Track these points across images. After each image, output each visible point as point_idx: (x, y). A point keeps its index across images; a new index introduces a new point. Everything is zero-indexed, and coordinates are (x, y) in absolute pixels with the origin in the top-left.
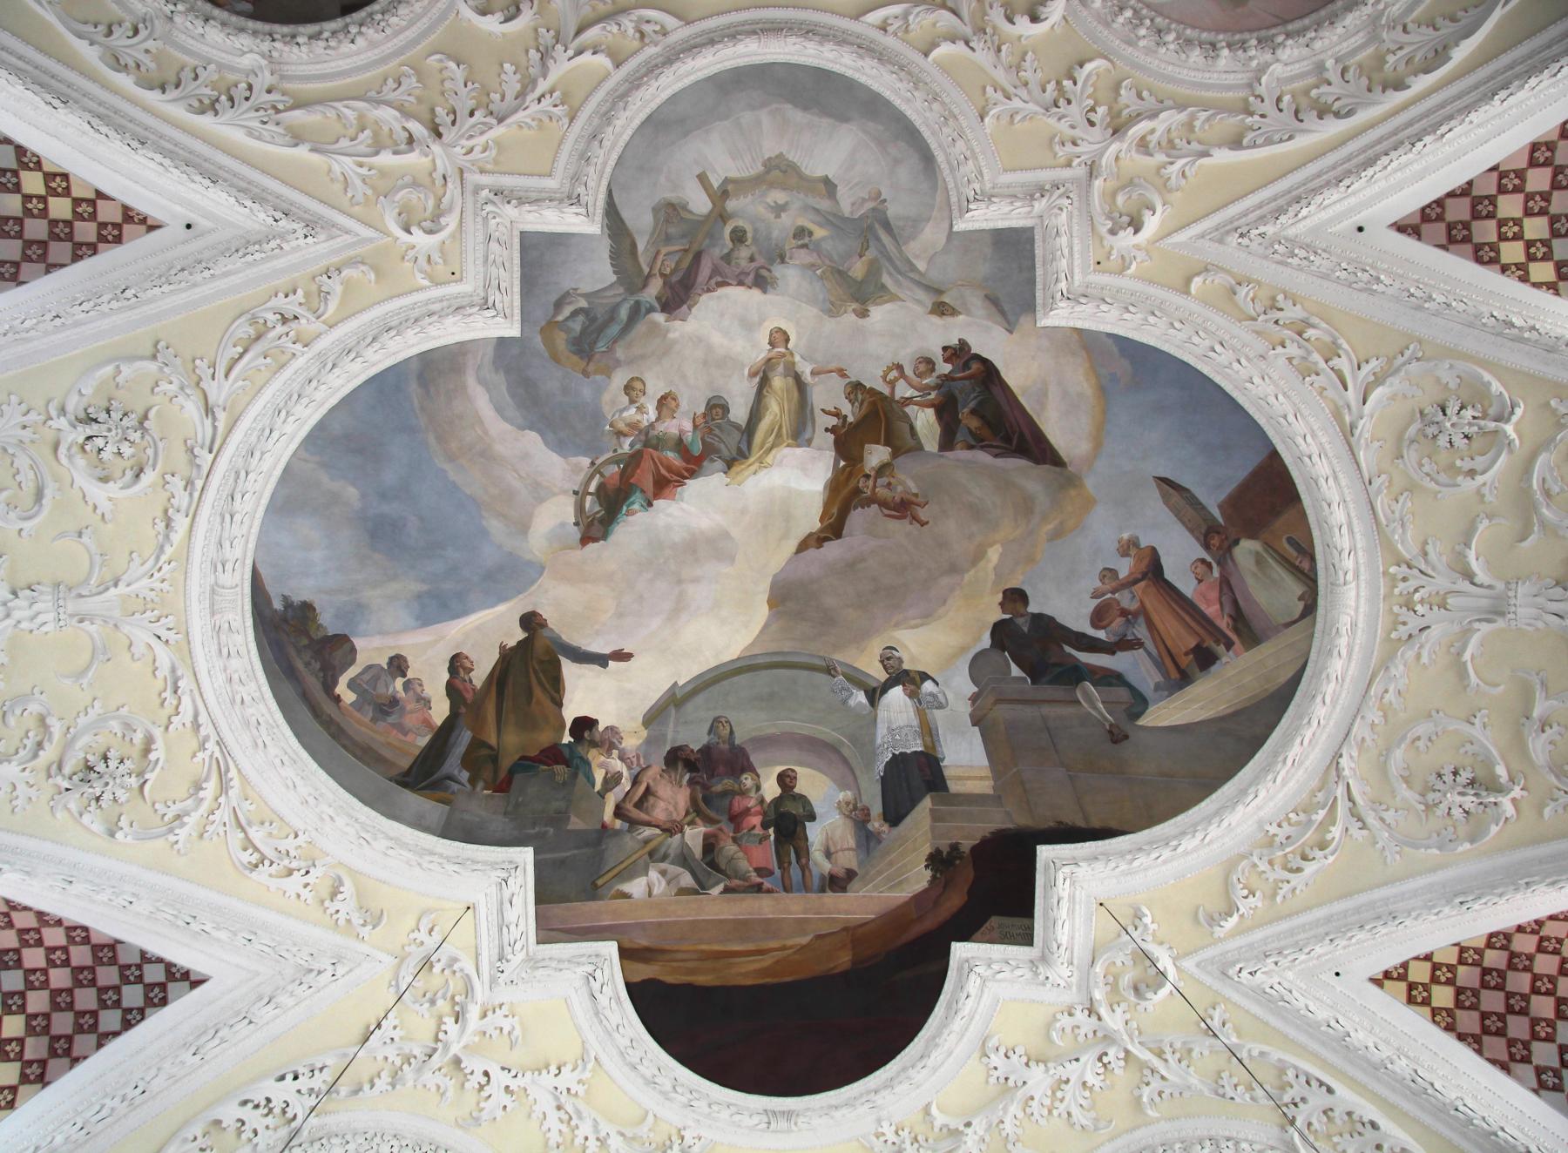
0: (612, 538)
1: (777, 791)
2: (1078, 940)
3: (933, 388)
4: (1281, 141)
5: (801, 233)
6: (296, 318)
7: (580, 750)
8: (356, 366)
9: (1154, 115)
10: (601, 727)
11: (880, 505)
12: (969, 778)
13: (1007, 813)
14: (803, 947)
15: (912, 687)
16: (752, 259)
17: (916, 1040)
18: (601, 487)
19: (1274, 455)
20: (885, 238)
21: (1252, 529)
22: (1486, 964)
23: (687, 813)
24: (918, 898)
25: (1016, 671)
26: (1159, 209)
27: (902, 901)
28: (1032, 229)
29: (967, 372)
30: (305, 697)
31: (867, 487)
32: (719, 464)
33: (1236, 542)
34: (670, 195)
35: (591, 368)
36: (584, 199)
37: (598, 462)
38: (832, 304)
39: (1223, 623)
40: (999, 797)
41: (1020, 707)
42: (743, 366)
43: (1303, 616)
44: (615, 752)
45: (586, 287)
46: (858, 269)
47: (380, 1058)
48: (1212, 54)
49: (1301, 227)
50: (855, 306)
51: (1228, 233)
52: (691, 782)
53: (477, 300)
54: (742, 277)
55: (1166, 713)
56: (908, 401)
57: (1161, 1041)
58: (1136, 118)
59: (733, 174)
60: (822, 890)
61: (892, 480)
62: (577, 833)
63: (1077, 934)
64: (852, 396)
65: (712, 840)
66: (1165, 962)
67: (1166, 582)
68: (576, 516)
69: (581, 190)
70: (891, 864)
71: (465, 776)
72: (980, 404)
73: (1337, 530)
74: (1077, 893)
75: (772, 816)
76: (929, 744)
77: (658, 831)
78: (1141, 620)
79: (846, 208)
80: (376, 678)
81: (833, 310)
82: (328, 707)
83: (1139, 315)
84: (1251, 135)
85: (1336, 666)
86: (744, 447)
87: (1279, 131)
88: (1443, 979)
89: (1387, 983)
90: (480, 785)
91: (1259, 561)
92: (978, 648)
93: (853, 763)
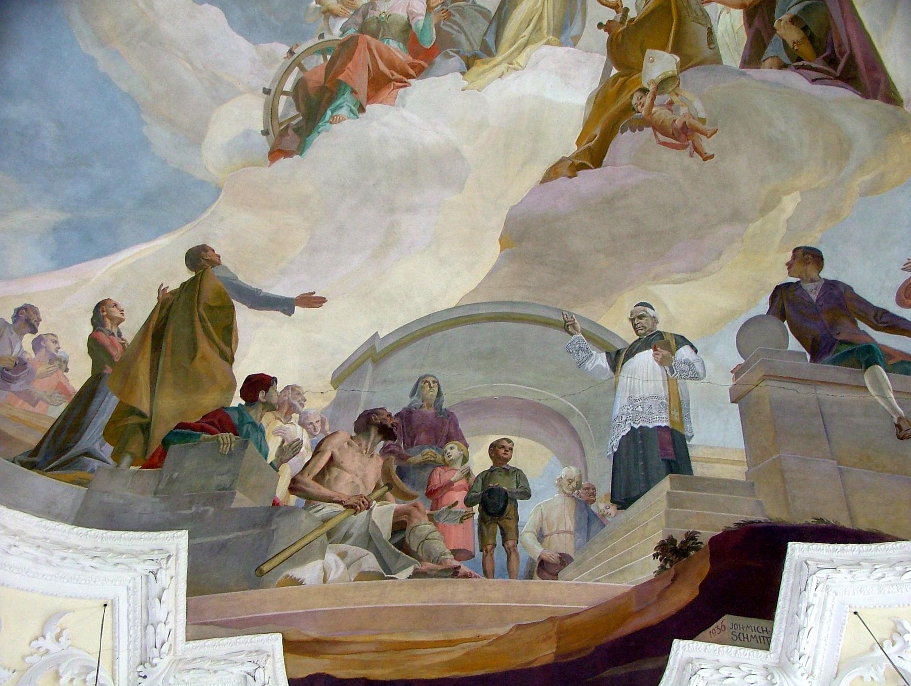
1: (488, 464)
7: (253, 414)
10: (280, 387)
11: (654, 129)
12: (718, 461)
13: (760, 504)
14: (500, 638)
15: (665, 352)
23: (377, 487)
24: (640, 590)
25: (794, 344)
31: (641, 104)
32: (456, 61)
37: (298, 51)
40: (753, 484)
41: (794, 386)
52: (385, 451)
60: (530, 576)
61: (675, 99)
63: (822, 643)
65: (404, 518)
68: (265, 123)
70: (613, 550)
71: (107, 450)
74: (830, 599)
75: (479, 490)
76: (677, 419)
77: (340, 508)
86: (490, 40)
90: (127, 459)
92: (753, 313)
93: (582, 434)
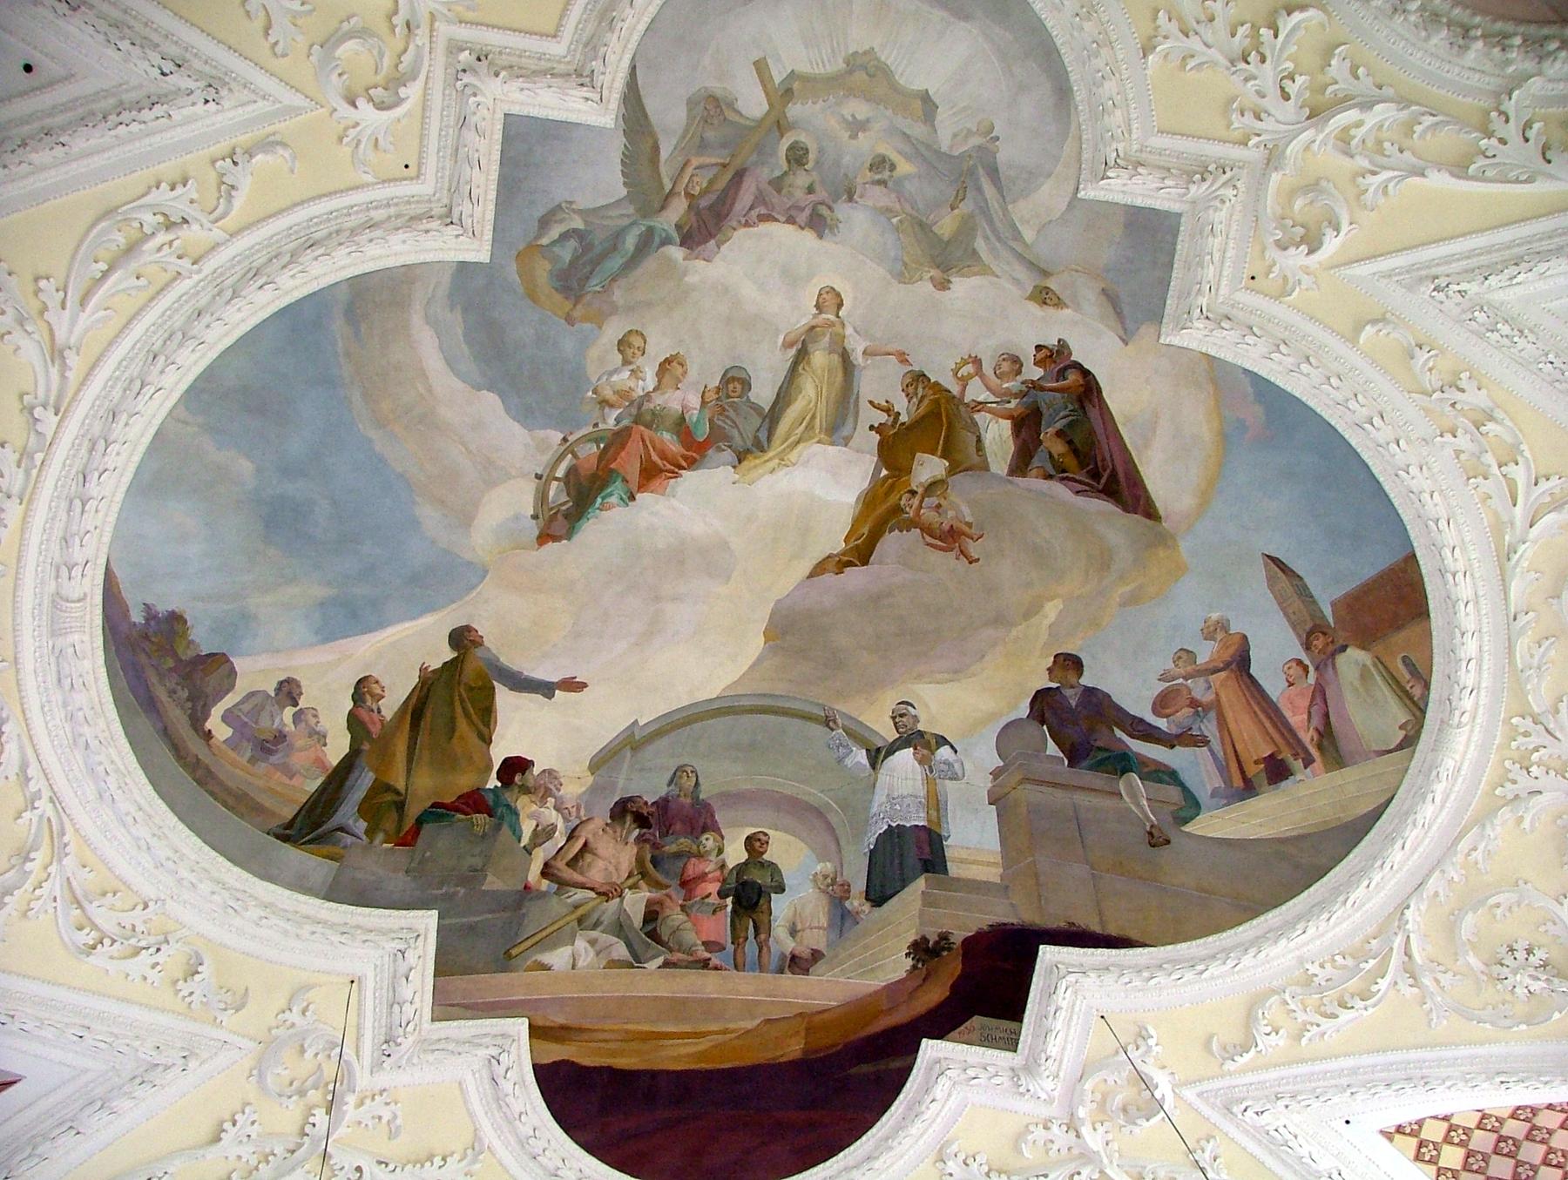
0: (577, 538)
1: (744, 856)
2: (1070, 1053)
3: (1016, 396)
4: (1517, 181)
5: (880, 163)
6: (185, 221)
7: (508, 796)
8: (267, 294)
9: (1367, 106)
10: (536, 770)
12: (974, 862)
14: (748, 1031)
15: (925, 752)
16: (810, 190)
17: (864, 1138)
18: (572, 471)
19: (1412, 558)
20: (989, 190)
21: (1366, 637)
22: (1504, 1132)
25: (1052, 749)
26: (1345, 228)
27: (871, 990)
28: (1180, 215)
29: (1061, 383)
30: (166, 733)
31: (910, 506)
32: (728, 455)
33: (1344, 648)
34: (715, 86)
35: (578, 312)
36: (599, 80)
37: (571, 439)
38: (905, 265)
39: (1307, 737)
40: (1007, 887)
42: (777, 331)
43: (1400, 747)
44: (551, 800)
45: (585, 201)
46: (946, 225)
47: (232, 1158)
48: (1461, 42)
49: (1510, 295)
50: (933, 272)
51: (1421, 280)
52: (640, 840)
53: (438, 210)
54: (793, 213)
55: (1216, 823)
56: (979, 406)
57: (1145, 1167)
58: (1343, 102)
59: (804, 68)
61: (943, 502)
62: (493, 894)
64: (911, 389)
65: (656, 908)
66: (1164, 1089)
67: (1250, 676)
69: (596, 65)
70: (866, 947)
71: (361, 826)
72: (1071, 425)
73: (1464, 664)
74: (1078, 1002)
77: (592, 894)
78: (1212, 715)
79: (945, 141)
80: (257, 711)
81: (904, 275)
82: (195, 745)
83: (1290, 360)
84: (1481, 162)
85: (1427, 811)
86: (763, 436)
87: (1518, 166)
88: (1456, 1140)
89: (1397, 1137)
90: (380, 836)
91: (1364, 675)
